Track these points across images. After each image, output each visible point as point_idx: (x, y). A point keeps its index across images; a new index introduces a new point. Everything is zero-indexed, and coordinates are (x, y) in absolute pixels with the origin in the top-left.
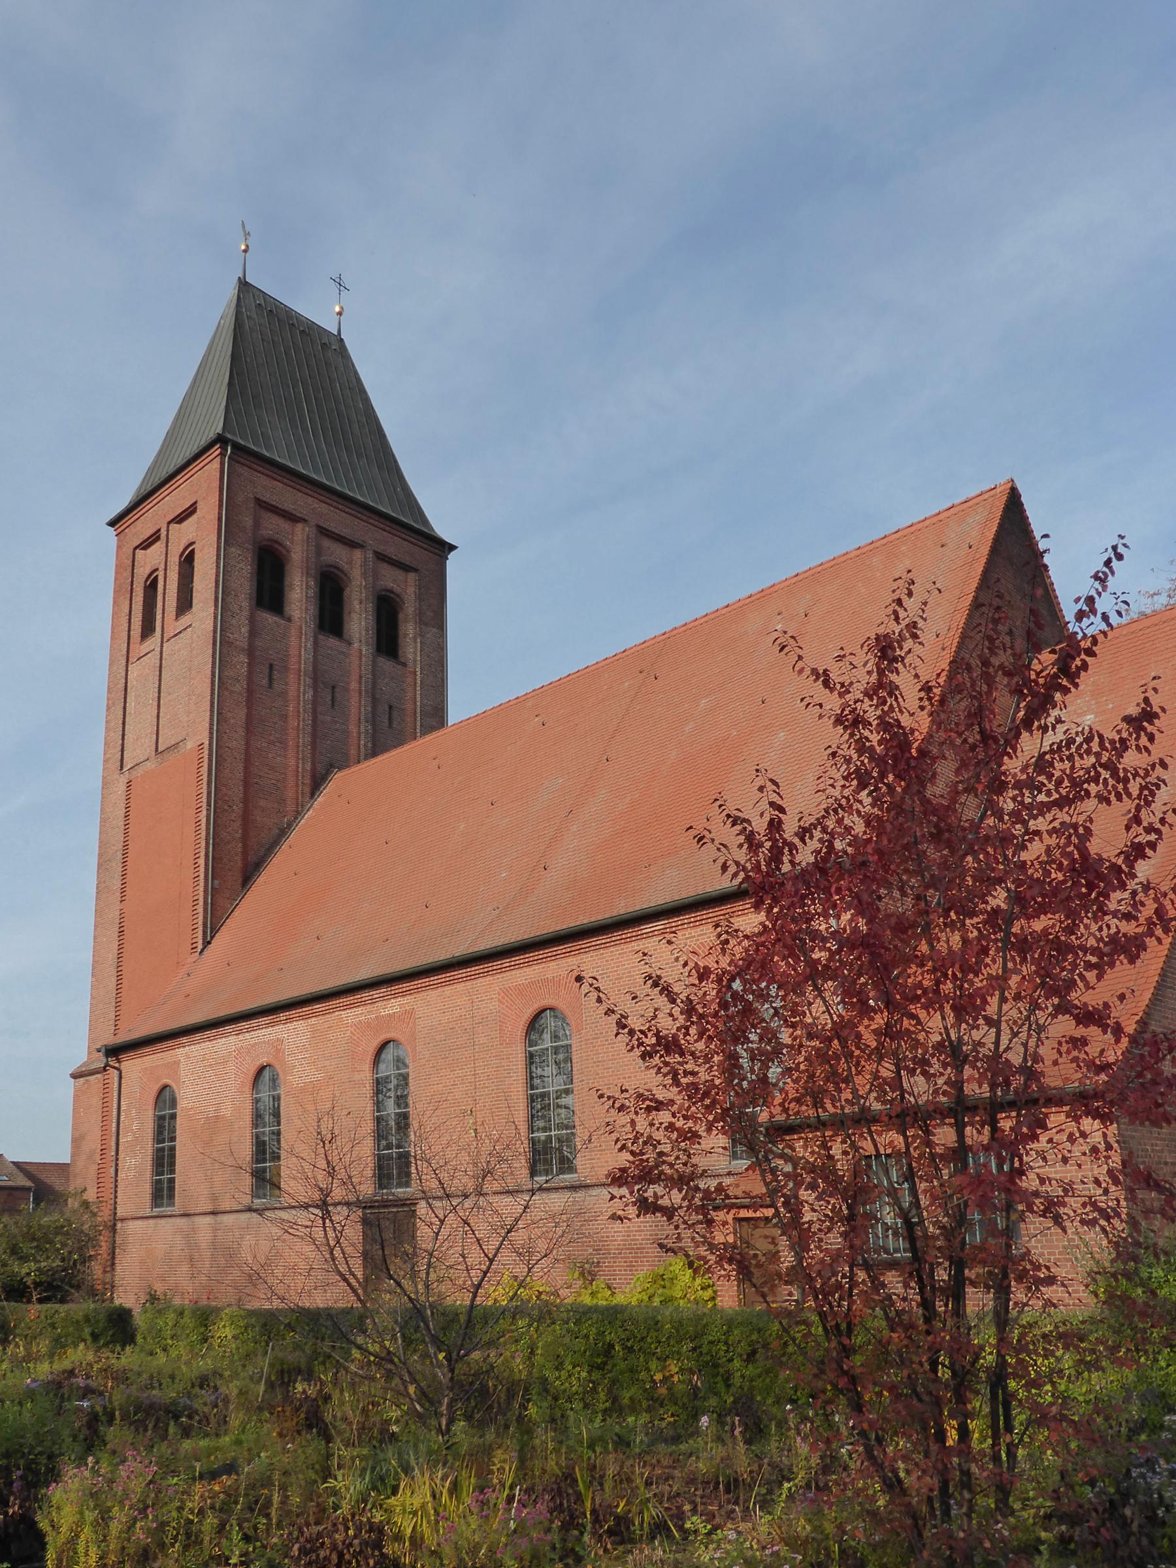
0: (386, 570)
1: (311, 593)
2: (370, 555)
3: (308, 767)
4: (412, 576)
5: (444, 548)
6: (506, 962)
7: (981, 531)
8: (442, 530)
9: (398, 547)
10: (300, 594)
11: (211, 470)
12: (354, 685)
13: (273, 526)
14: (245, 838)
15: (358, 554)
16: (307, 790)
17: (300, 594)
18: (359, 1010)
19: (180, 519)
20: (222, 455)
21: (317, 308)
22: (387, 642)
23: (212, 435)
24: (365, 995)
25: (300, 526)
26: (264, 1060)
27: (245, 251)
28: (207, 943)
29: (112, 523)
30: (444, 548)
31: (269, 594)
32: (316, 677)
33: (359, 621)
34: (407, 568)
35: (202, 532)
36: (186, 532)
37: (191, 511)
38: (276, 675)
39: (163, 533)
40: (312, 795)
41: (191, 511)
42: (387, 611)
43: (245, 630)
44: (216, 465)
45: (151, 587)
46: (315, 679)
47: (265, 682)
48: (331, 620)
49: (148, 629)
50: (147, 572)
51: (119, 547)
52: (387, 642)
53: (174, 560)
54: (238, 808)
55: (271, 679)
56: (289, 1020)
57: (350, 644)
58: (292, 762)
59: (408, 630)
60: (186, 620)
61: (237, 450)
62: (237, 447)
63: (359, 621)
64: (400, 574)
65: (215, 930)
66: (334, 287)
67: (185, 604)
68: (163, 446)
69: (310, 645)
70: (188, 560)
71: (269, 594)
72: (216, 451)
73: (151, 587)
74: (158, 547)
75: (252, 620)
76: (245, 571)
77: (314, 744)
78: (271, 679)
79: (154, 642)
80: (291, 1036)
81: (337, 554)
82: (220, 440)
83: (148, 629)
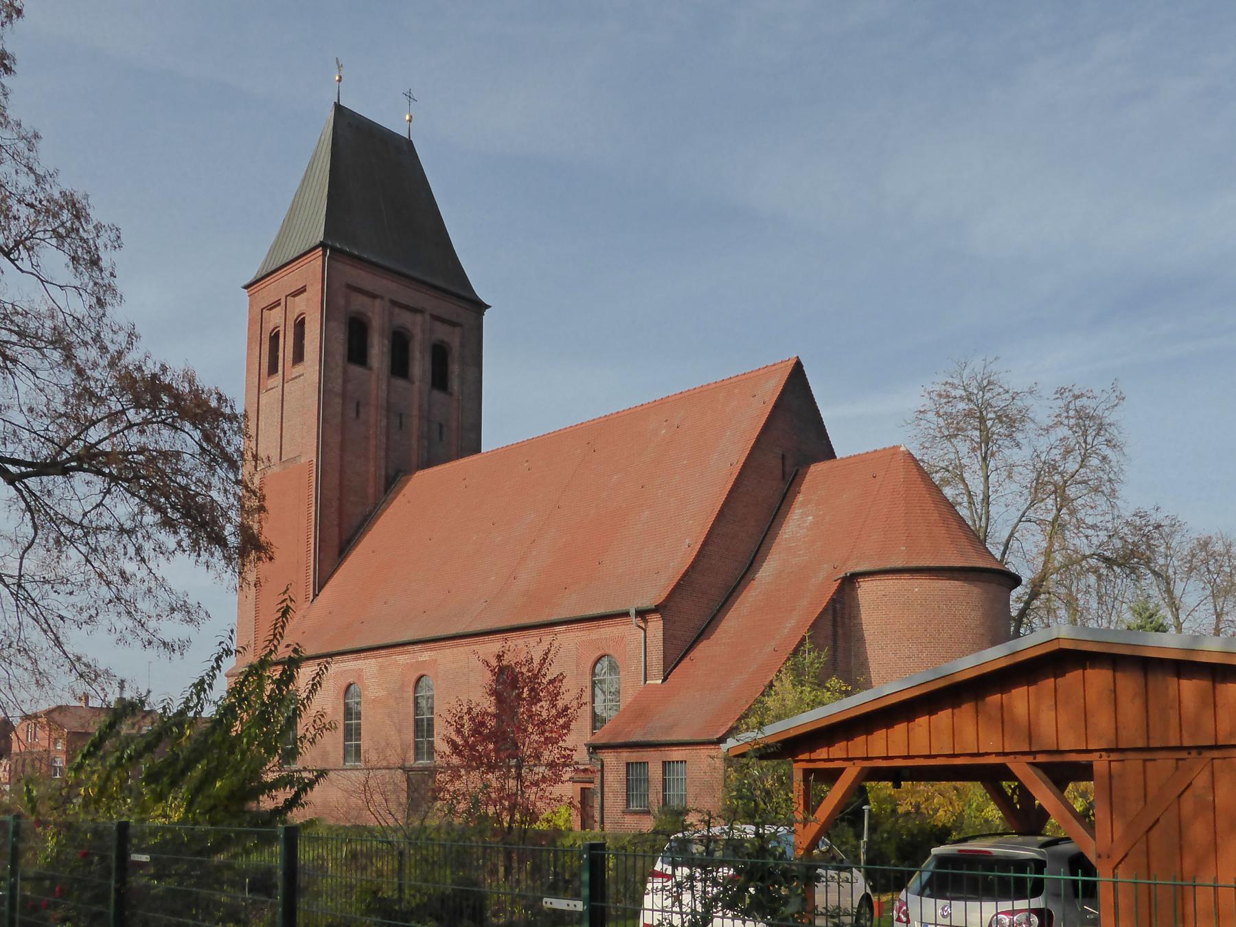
0: (439, 326)
1: (385, 350)
2: (428, 317)
3: (383, 473)
4: (457, 330)
5: (481, 307)
6: (486, 638)
7: (772, 389)
8: (481, 292)
9: (447, 308)
10: (378, 350)
11: (316, 263)
12: (415, 412)
13: (359, 303)
14: (340, 525)
15: (419, 317)
16: (382, 489)
17: (378, 350)
18: (406, 657)
19: (296, 294)
20: (324, 255)
21: (393, 120)
22: (440, 380)
23: (318, 242)
24: (410, 648)
25: (378, 301)
26: (351, 680)
27: (340, 81)
28: (315, 596)
29: (246, 287)
30: (481, 307)
31: (357, 353)
32: (389, 408)
33: (420, 365)
34: (454, 324)
35: (310, 306)
36: (300, 305)
37: (302, 290)
38: (362, 410)
39: (283, 303)
40: (386, 491)
41: (302, 290)
42: (440, 355)
43: (340, 381)
44: (319, 262)
45: (274, 338)
46: (388, 409)
47: (354, 415)
48: (400, 366)
49: (273, 369)
50: (272, 327)
51: (251, 305)
52: (440, 380)
53: (291, 324)
54: (335, 504)
55: (358, 412)
56: (366, 658)
57: (413, 383)
58: (372, 469)
59: (455, 369)
60: (299, 369)
61: (336, 245)
62: (333, 249)
63: (420, 365)
64: (448, 328)
65: (321, 588)
66: (405, 100)
67: (299, 357)
68: (278, 238)
69: (384, 387)
70: (300, 325)
71: (357, 353)
72: (319, 251)
73: (274, 338)
74: (278, 311)
75: (345, 372)
76: (340, 336)
77: (387, 456)
78: (358, 412)
79: (276, 380)
80: (368, 666)
81: (405, 319)
82: (323, 245)
83: (273, 369)
